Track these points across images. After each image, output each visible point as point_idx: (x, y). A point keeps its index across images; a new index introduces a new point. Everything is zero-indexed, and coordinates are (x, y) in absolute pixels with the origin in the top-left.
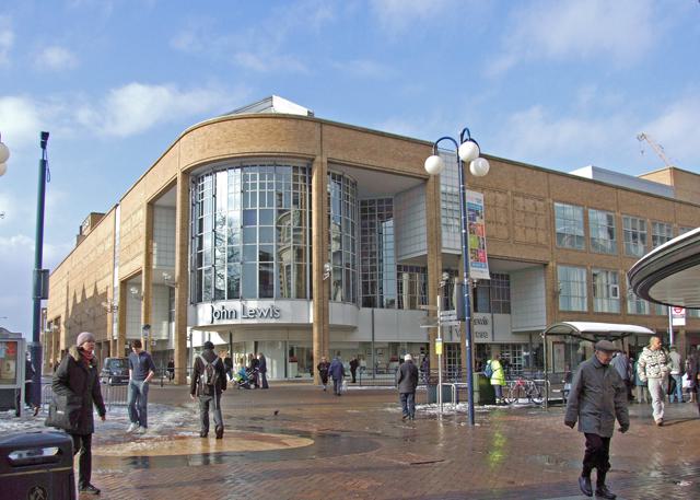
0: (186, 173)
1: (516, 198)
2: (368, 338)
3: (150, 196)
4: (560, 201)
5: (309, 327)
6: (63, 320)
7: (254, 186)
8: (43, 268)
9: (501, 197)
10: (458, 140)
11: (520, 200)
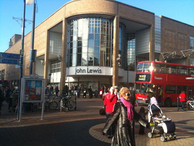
3: (49, 27)
4: (192, 36)
5: (110, 77)
6: (5, 71)
7: (93, 25)
11: (179, 35)
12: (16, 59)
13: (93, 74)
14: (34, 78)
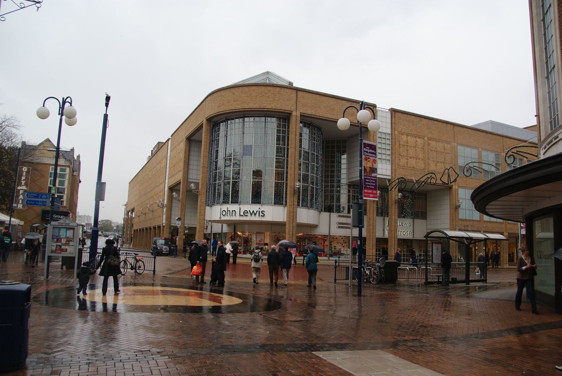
0: (209, 120)
1: (430, 142)
2: (326, 233)
8: (103, 181)
9: (420, 141)
10: (359, 108)
11: (433, 143)
12: (44, 200)
13: (249, 218)
14: (64, 225)
